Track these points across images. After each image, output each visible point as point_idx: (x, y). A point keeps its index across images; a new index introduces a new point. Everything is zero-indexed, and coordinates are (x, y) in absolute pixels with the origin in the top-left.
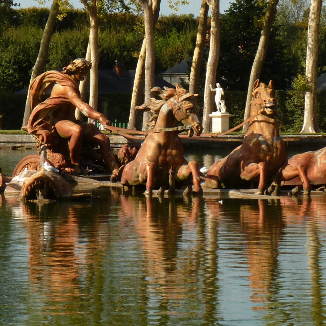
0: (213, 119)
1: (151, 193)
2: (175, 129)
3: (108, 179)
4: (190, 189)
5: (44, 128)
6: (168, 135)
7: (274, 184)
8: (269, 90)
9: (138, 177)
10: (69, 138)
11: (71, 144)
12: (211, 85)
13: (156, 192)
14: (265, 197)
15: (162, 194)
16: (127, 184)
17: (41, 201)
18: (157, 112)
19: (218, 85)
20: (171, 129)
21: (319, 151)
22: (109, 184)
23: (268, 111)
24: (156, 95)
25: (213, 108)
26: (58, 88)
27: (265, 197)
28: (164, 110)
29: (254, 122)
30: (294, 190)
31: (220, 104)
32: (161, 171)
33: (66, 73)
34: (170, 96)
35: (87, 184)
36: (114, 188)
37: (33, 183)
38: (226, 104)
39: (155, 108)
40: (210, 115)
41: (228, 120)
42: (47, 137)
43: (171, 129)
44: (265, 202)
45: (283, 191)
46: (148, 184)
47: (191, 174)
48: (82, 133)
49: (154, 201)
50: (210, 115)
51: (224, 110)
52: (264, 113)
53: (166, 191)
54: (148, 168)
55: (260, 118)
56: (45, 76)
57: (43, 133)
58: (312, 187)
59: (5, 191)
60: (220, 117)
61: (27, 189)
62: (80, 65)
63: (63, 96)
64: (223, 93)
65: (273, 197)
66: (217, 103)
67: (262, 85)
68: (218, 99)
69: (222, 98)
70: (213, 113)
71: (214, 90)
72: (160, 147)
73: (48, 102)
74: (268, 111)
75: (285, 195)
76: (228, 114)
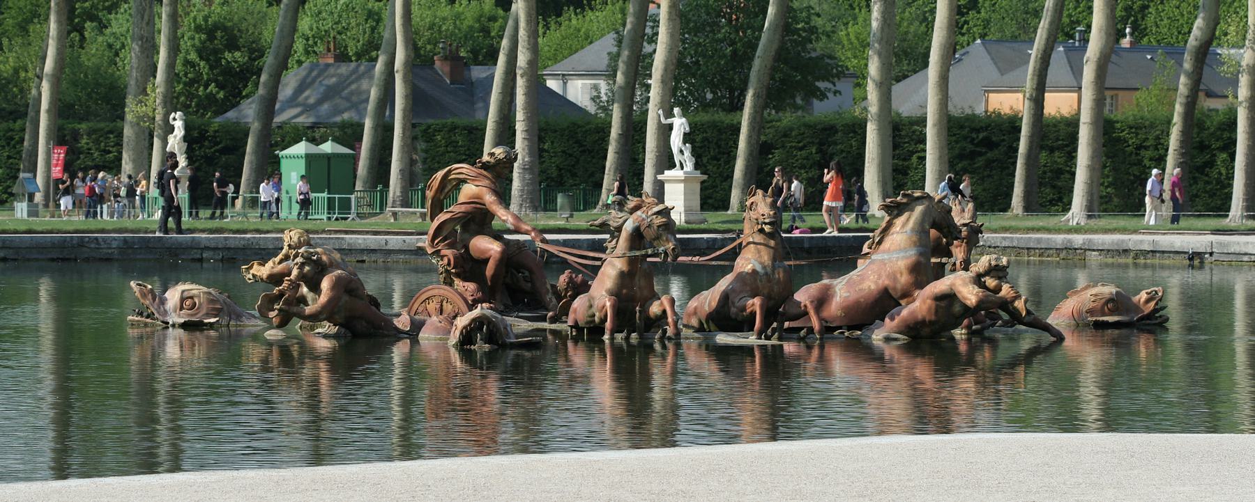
0: (666, 186)
1: (612, 339)
2: (643, 252)
3: (543, 319)
4: (665, 331)
5: (450, 246)
6: (632, 261)
7: (775, 325)
8: (769, 200)
9: (594, 316)
10: (486, 261)
11: (490, 270)
12: (661, 112)
13: (619, 337)
14: (763, 342)
15: (627, 338)
16: (575, 326)
17: (481, 347)
18: (619, 229)
19: (676, 110)
20: (638, 253)
21: (839, 280)
22: (546, 325)
23: (767, 228)
24: (621, 205)
25: (667, 161)
26: (468, 190)
27: (763, 342)
28: (629, 226)
29: (749, 243)
30: (802, 333)
31: (681, 152)
32: (630, 303)
33: (481, 168)
34: (637, 208)
35: (520, 325)
36: (553, 332)
37: (470, 324)
38: (694, 153)
39: (615, 225)
40: (660, 177)
41: (698, 187)
42: (455, 258)
43: (638, 253)
44: (762, 347)
45: (787, 334)
46: (608, 325)
47: (664, 312)
48: (503, 253)
49: (617, 350)
50: (660, 177)
51: (689, 166)
52: (761, 231)
53: (634, 335)
54: (608, 304)
55: (758, 238)
56: (450, 171)
57: (449, 253)
58: (828, 329)
59: (421, 335)
60: (681, 181)
61: (461, 333)
62: (502, 156)
63: (476, 201)
64: (688, 129)
65: (774, 342)
66: (675, 150)
67: (760, 192)
68: (676, 140)
69: (687, 138)
70: (667, 172)
71: (669, 121)
72: (622, 275)
73: (456, 209)
74: (767, 228)
75: (789, 340)
76: (698, 174)
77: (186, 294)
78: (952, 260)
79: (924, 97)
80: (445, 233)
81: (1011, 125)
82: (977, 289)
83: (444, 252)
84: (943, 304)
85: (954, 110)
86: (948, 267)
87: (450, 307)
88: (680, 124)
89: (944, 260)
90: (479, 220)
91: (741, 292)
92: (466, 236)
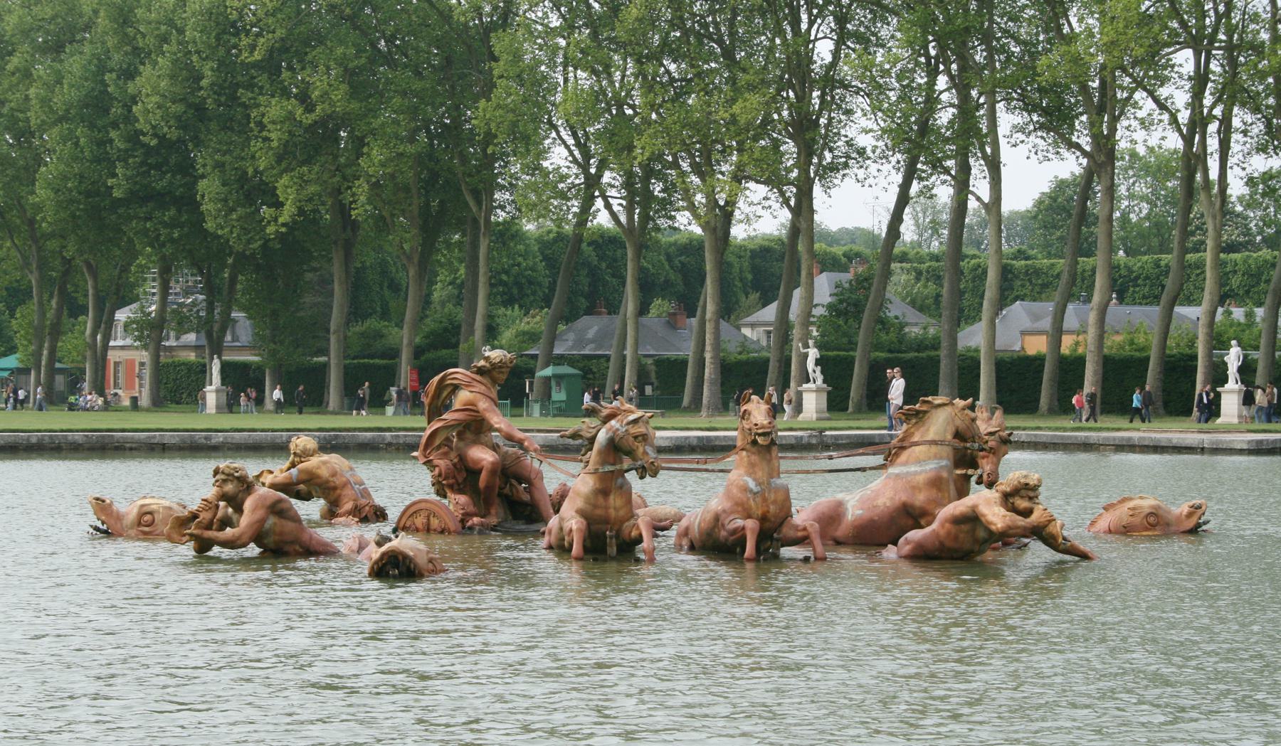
10: (480, 471)
25: (806, 379)
26: (463, 396)
28: (602, 436)
33: (477, 373)
39: (589, 435)
63: (470, 408)
66: (810, 371)
68: (810, 364)
69: (818, 362)
77: (146, 509)
78: (979, 472)
79: (973, 337)
80: (437, 442)
81: (1038, 361)
82: (1003, 511)
83: (436, 462)
84: (965, 527)
85: (999, 345)
86: (973, 479)
87: (437, 521)
88: (813, 353)
89: (970, 472)
90: (475, 427)
91: (732, 513)
92: (461, 444)
